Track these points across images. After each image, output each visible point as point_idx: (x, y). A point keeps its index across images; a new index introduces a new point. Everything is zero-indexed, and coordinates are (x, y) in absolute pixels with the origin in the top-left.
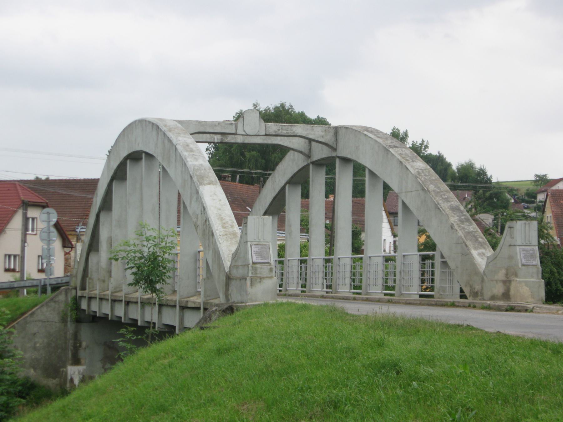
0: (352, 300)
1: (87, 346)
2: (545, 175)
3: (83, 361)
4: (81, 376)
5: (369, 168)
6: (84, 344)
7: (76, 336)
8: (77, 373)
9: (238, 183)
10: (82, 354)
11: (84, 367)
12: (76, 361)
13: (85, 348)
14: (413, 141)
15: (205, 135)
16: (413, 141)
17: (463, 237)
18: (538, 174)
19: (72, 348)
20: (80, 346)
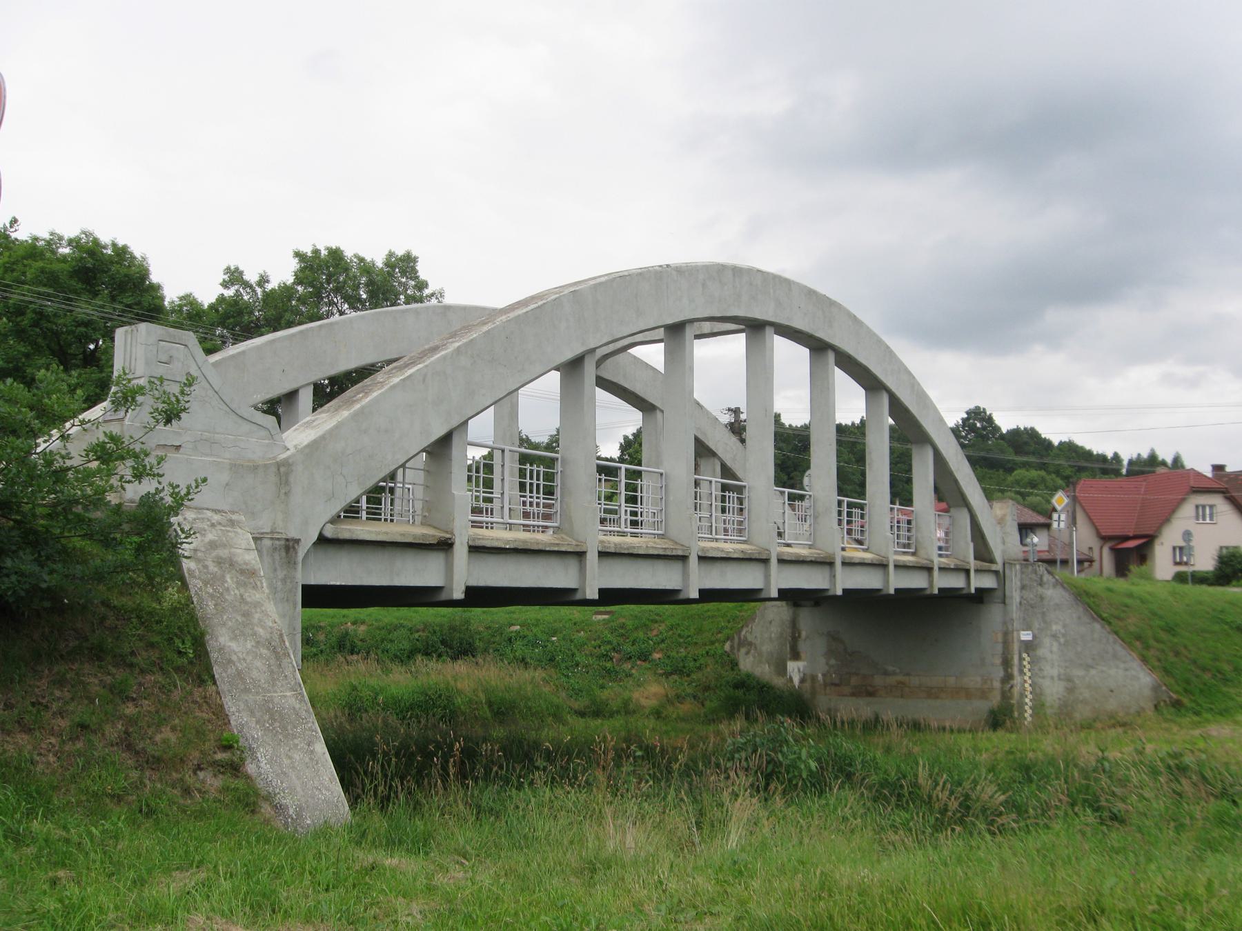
0: (1211, 584)
1: (807, 637)
2: (391, 254)
3: (803, 655)
4: (802, 675)
5: (362, 492)
6: (804, 634)
7: (794, 624)
8: (796, 670)
9: (620, 468)
10: (803, 646)
11: (805, 663)
12: (796, 656)
13: (805, 640)
14: (14, 221)
15: (657, 330)
16: (14, 221)
17: (1153, 849)
18: (362, 254)
19: (790, 639)
20: (799, 636)
